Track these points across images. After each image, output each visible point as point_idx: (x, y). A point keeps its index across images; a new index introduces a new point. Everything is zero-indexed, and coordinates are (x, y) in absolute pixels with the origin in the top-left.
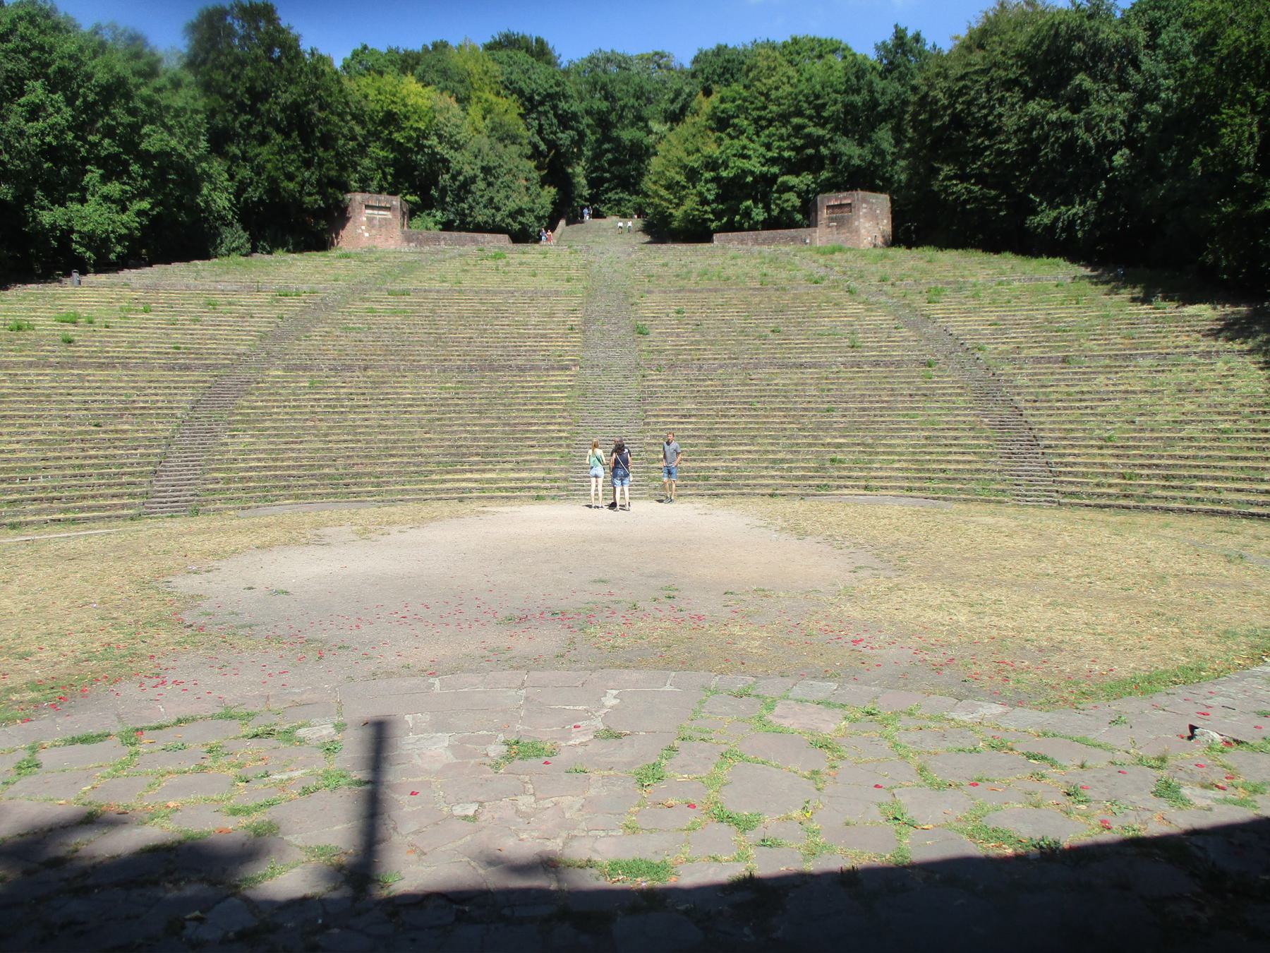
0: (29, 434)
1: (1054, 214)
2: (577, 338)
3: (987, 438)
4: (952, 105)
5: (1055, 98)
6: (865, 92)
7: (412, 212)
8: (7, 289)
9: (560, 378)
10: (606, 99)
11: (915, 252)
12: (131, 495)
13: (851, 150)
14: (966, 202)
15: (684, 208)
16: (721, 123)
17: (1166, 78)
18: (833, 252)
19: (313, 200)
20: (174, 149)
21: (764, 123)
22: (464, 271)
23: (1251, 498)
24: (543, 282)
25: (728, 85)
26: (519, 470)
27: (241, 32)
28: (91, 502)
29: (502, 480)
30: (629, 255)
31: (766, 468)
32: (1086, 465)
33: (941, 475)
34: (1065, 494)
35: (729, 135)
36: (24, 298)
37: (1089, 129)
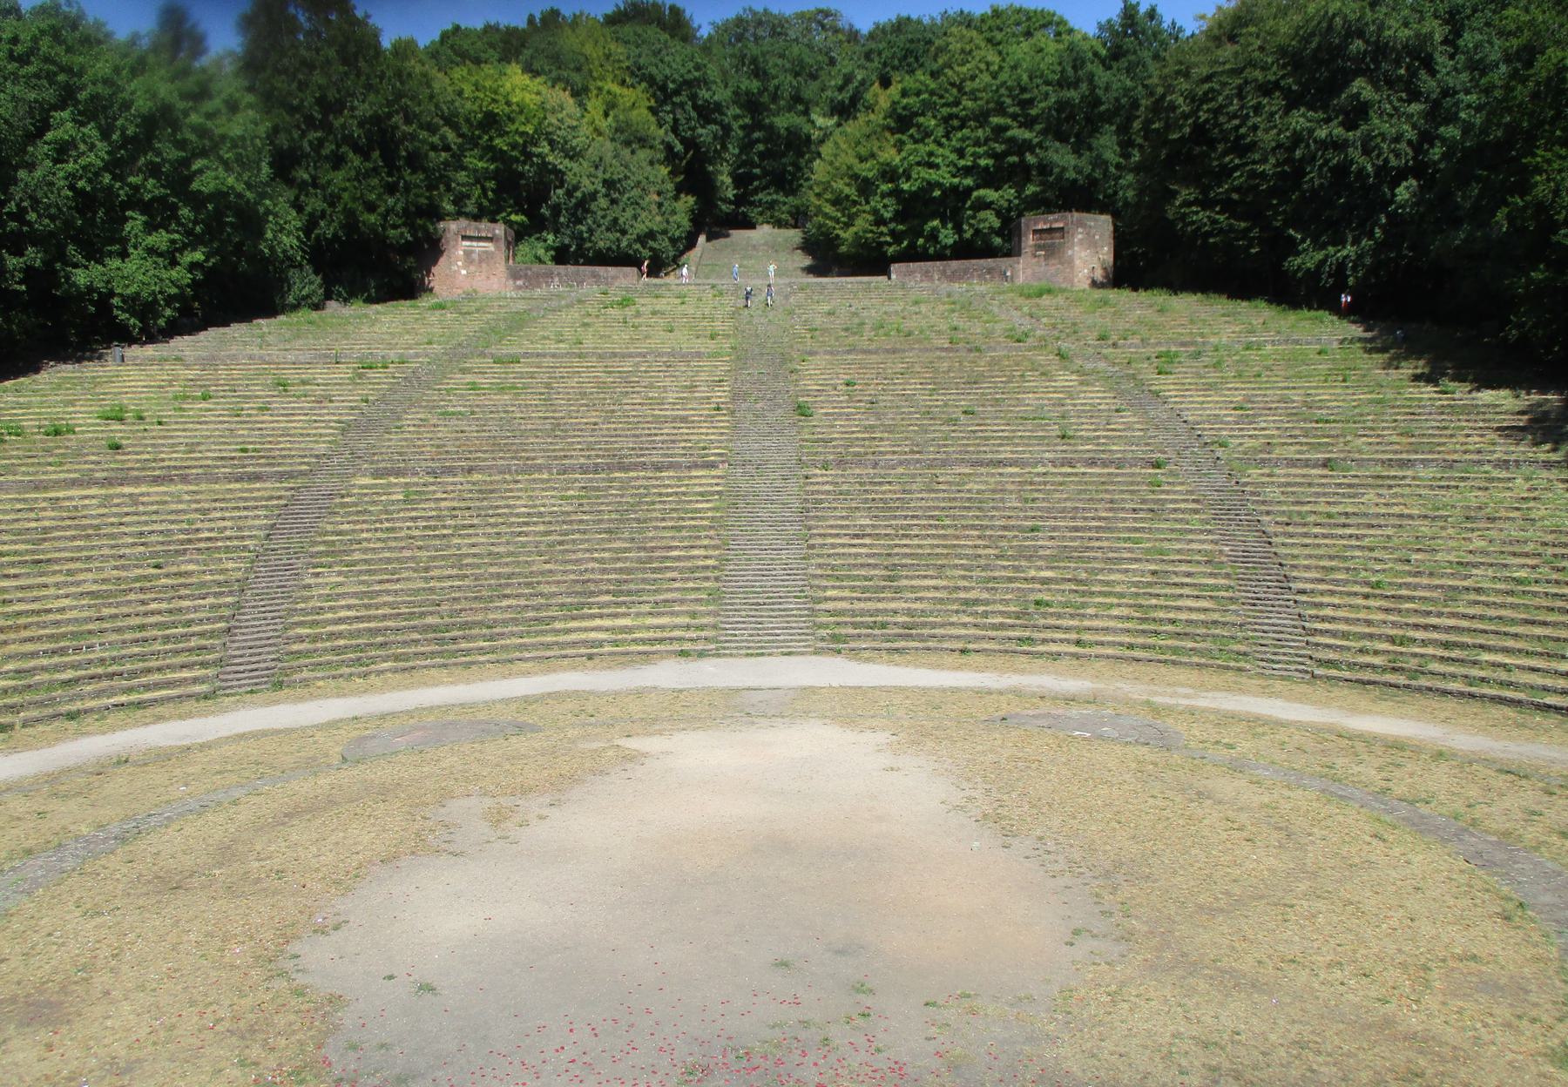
0: (78, 584)
1: (1320, 256)
2: (723, 421)
3: (1228, 576)
4: (1194, 113)
5: (1325, 108)
6: (1084, 86)
7: (519, 235)
8: (37, 371)
9: (703, 479)
10: (757, 75)
11: (1143, 296)
12: (204, 665)
13: (1063, 158)
14: (1209, 234)
15: (853, 230)
16: (902, 122)
17: (1467, 92)
18: (1040, 295)
19: (399, 234)
20: (232, 188)
21: (956, 123)
22: (585, 325)
23: (1549, 682)
24: (683, 341)
25: (912, 72)
26: (659, 614)
27: (307, 25)
28: (157, 677)
29: (639, 628)
30: (787, 297)
31: (957, 612)
32: (1347, 621)
33: (1170, 628)
34: (1322, 663)
35: (911, 136)
36: (59, 387)
37: (1366, 152)
